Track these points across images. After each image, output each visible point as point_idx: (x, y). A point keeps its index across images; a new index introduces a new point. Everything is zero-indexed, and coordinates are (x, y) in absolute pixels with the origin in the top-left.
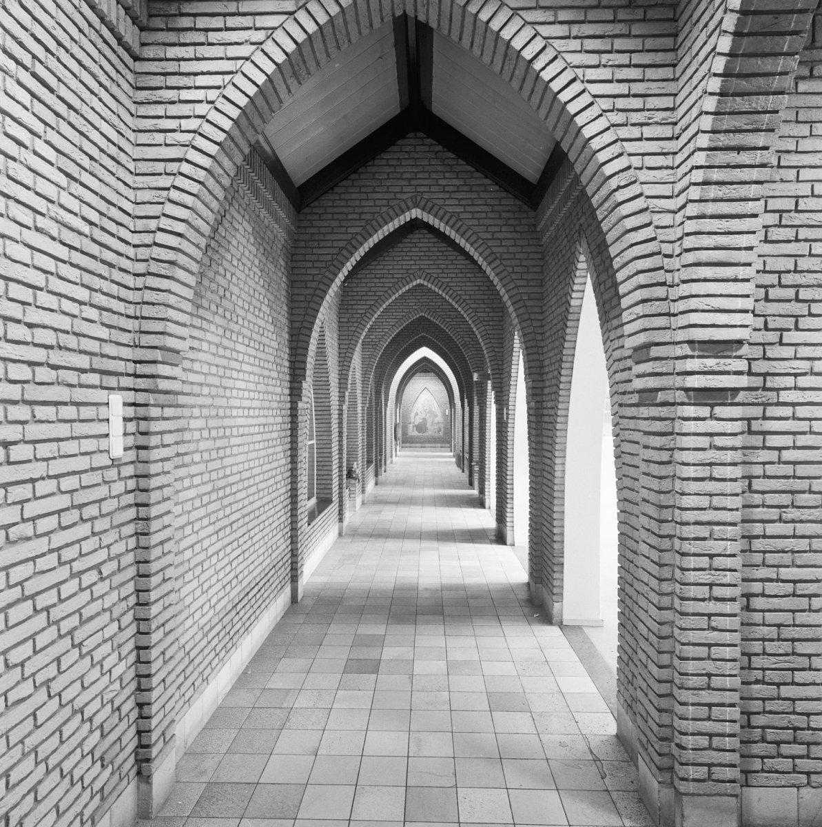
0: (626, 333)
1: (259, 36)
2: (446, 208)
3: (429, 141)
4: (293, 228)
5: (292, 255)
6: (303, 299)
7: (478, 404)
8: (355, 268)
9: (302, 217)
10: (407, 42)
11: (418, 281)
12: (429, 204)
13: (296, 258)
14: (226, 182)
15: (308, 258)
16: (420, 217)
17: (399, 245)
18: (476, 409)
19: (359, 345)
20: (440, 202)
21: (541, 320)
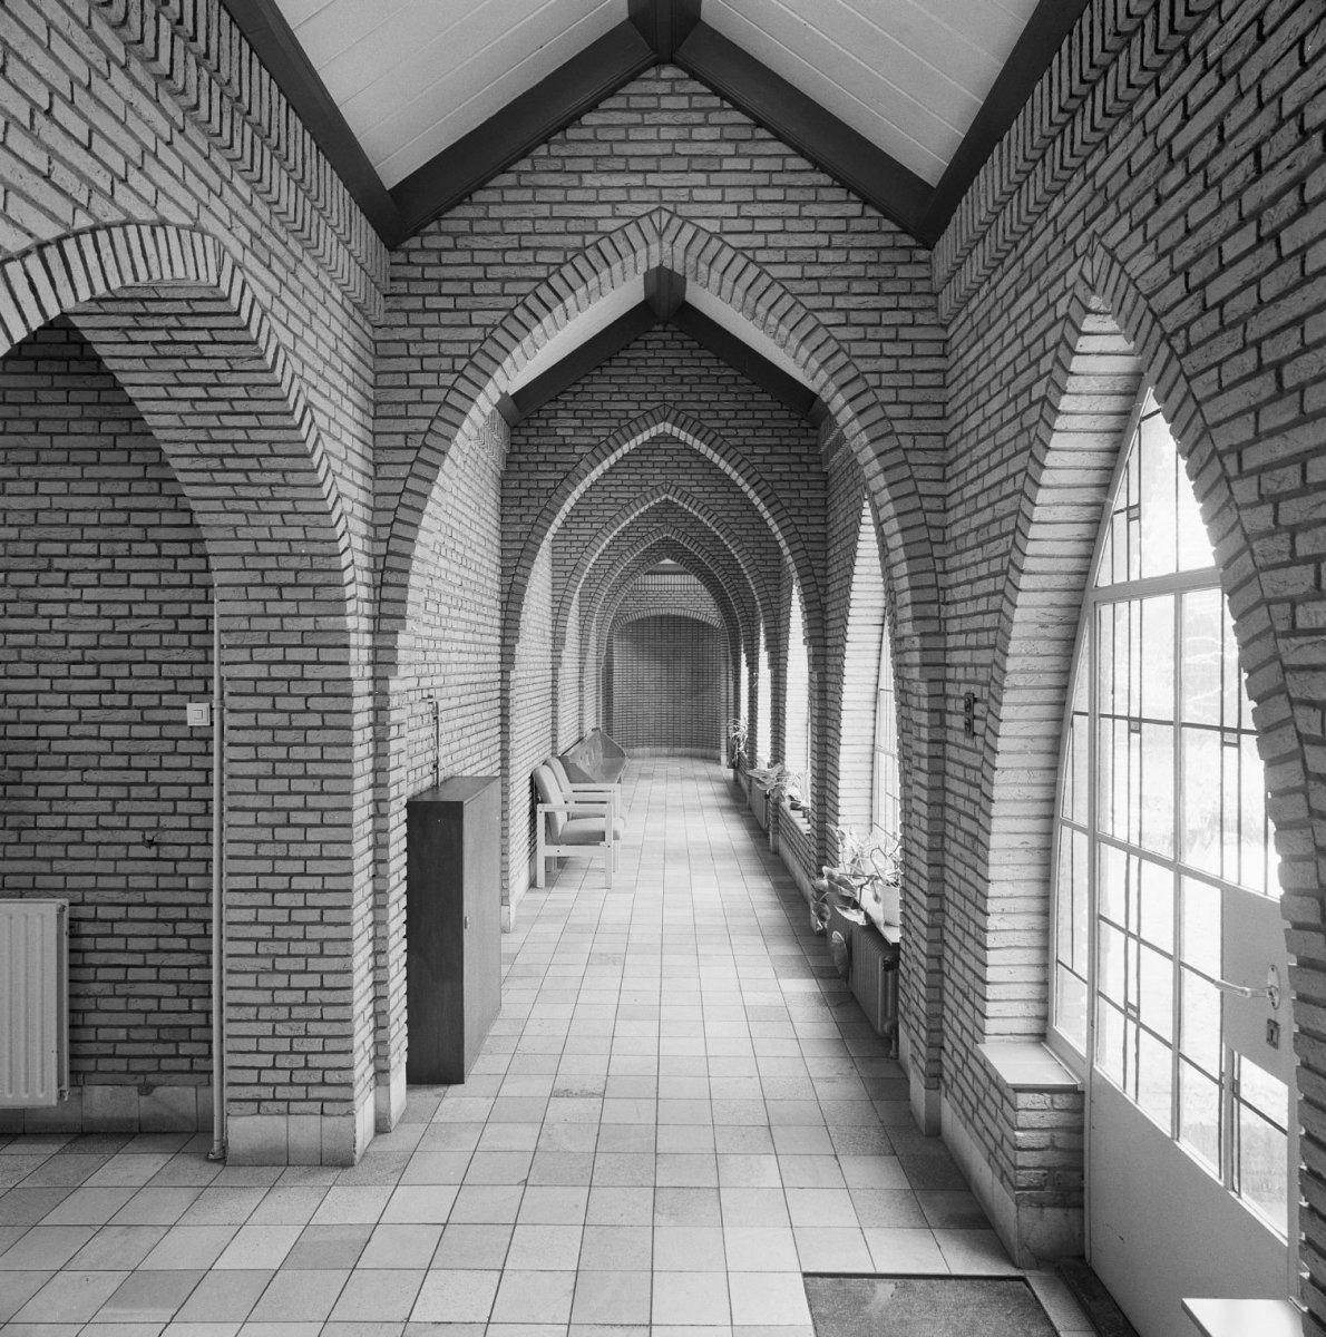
1: (511, 302)
2: (727, 238)
9: (400, 257)
18: (765, 673)
20: (695, 415)
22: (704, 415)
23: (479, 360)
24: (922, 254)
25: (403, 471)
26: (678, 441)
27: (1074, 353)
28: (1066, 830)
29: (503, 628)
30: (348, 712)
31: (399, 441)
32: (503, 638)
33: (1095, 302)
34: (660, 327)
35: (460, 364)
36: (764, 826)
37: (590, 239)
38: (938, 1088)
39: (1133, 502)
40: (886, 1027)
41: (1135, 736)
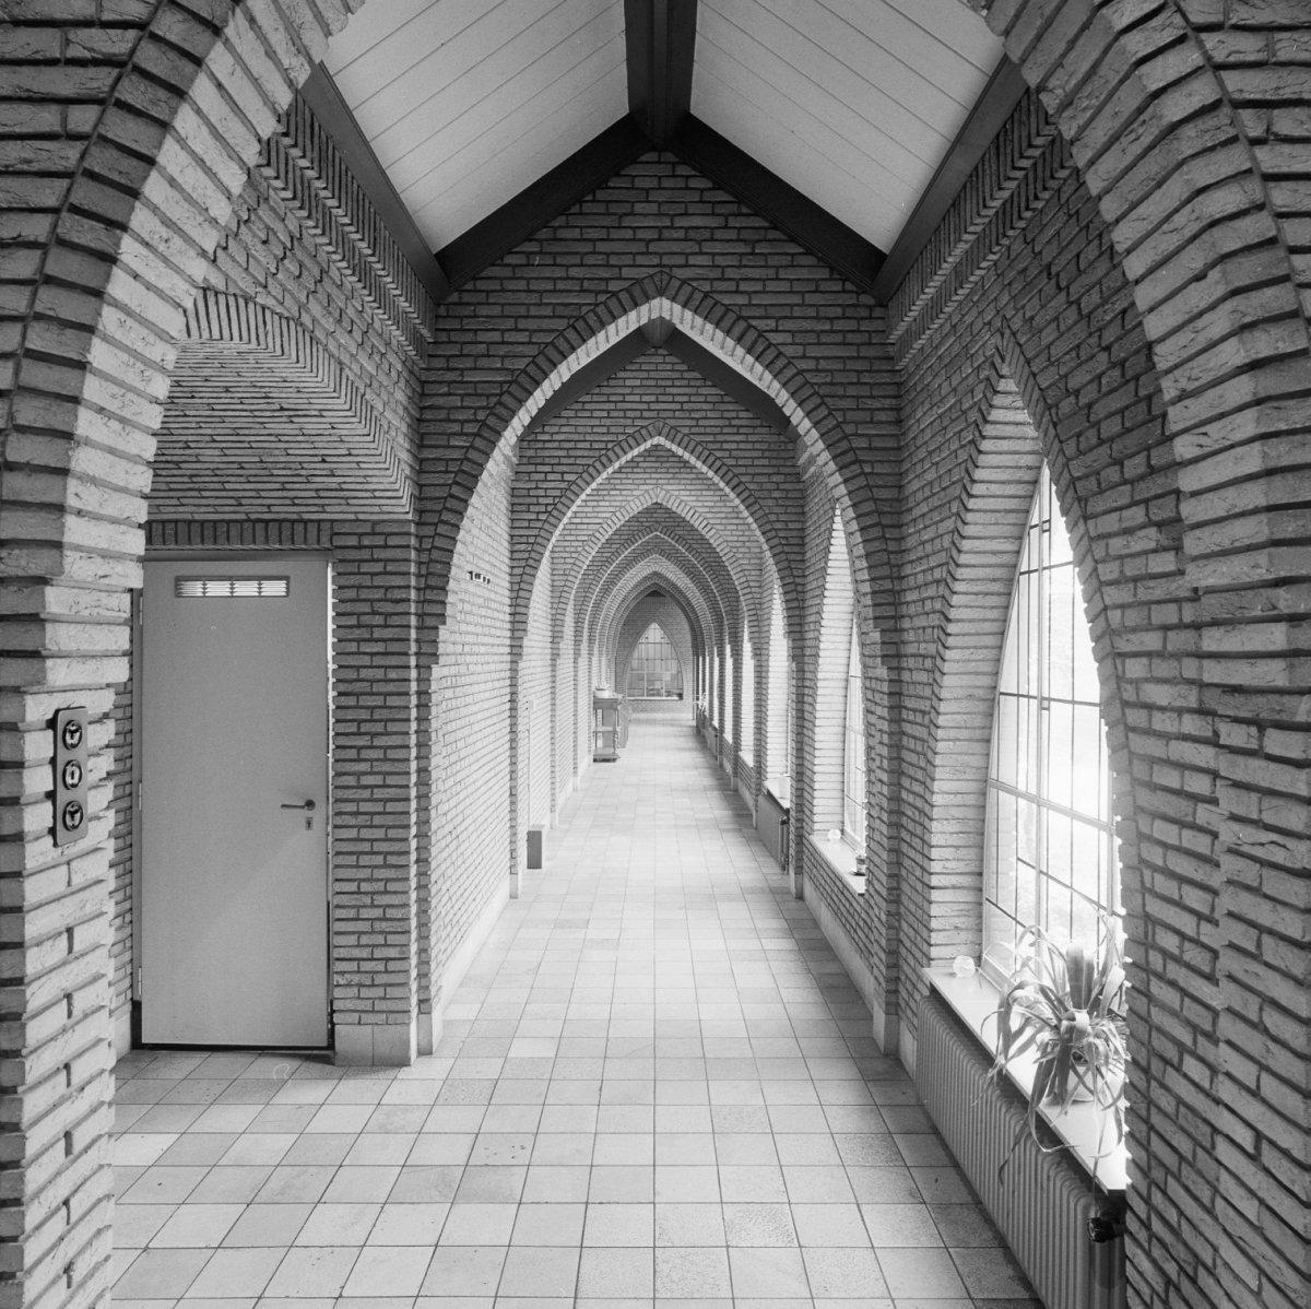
1: (580, 469)
2: (718, 297)
3: (683, 170)
4: (425, 332)
10: (651, 21)
11: (656, 440)
14: (235, 180)
17: (621, 374)
18: (729, 662)
23: (560, 506)
24: (878, 312)
26: (674, 455)
27: (996, 392)
28: (1104, 818)
30: (35, 655)
32: (513, 630)
35: (549, 508)
37: (602, 298)
39: (1046, 518)
41: (1045, 713)
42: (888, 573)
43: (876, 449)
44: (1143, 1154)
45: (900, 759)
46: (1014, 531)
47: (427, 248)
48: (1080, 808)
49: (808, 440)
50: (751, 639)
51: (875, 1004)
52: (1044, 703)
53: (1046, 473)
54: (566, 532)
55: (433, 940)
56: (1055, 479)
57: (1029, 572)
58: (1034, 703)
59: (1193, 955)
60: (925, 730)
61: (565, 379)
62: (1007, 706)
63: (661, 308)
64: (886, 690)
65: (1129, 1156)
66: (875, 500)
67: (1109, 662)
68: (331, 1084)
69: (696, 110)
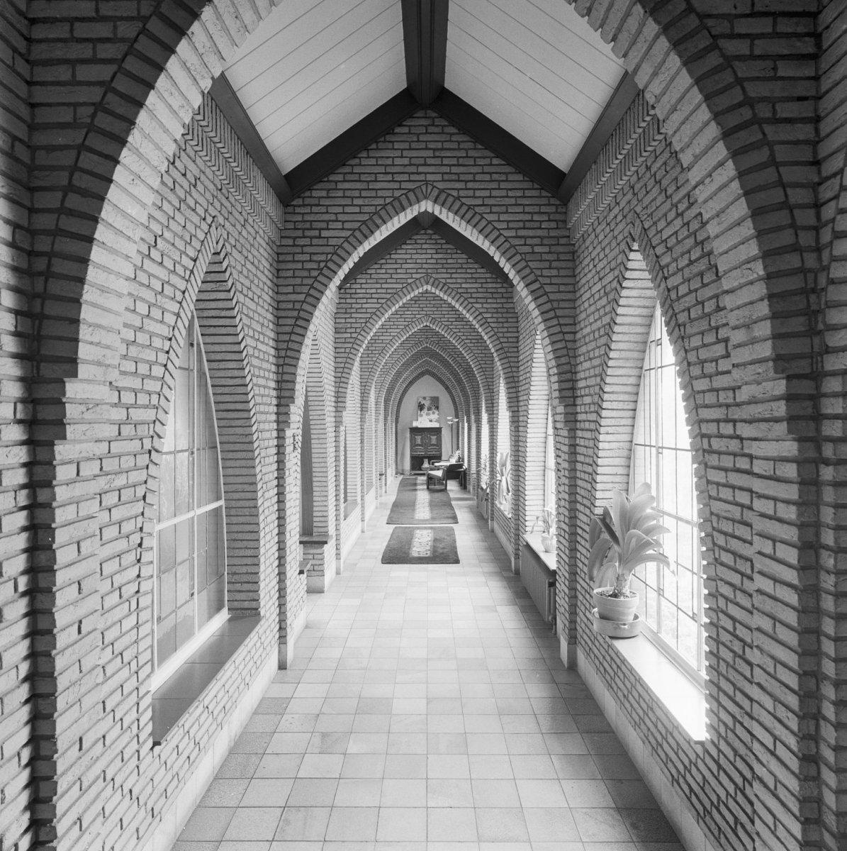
0: (712, 235)
5: (278, 270)
6: (291, 306)
7: (475, 421)
8: (351, 271)
9: (290, 209)
11: (425, 288)
12: (437, 282)
13: (282, 274)
15: (298, 257)
16: (430, 210)
19: (357, 364)
20: (455, 193)
21: (574, 284)
22: (462, 193)
25: (291, 321)
29: (278, 389)
31: (343, 350)
33: (636, 247)
34: (423, 232)
36: (486, 517)
38: (576, 643)
40: (550, 618)
41: (660, 455)
42: (566, 353)
43: (562, 292)
44: (715, 704)
45: (575, 478)
46: (640, 347)
47: (278, 170)
48: (681, 514)
49: (519, 288)
50: (487, 411)
51: (562, 637)
52: (660, 449)
53: (658, 312)
54: (373, 341)
55: (288, 598)
56: (664, 313)
57: (650, 369)
58: (654, 450)
59: (741, 598)
60: (589, 485)
61: (367, 250)
62: (640, 451)
63: (427, 206)
64: (567, 443)
65: (708, 706)
66: (560, 325)
67: (696, 426)
68: (233, 735)
69: (448, 85)
